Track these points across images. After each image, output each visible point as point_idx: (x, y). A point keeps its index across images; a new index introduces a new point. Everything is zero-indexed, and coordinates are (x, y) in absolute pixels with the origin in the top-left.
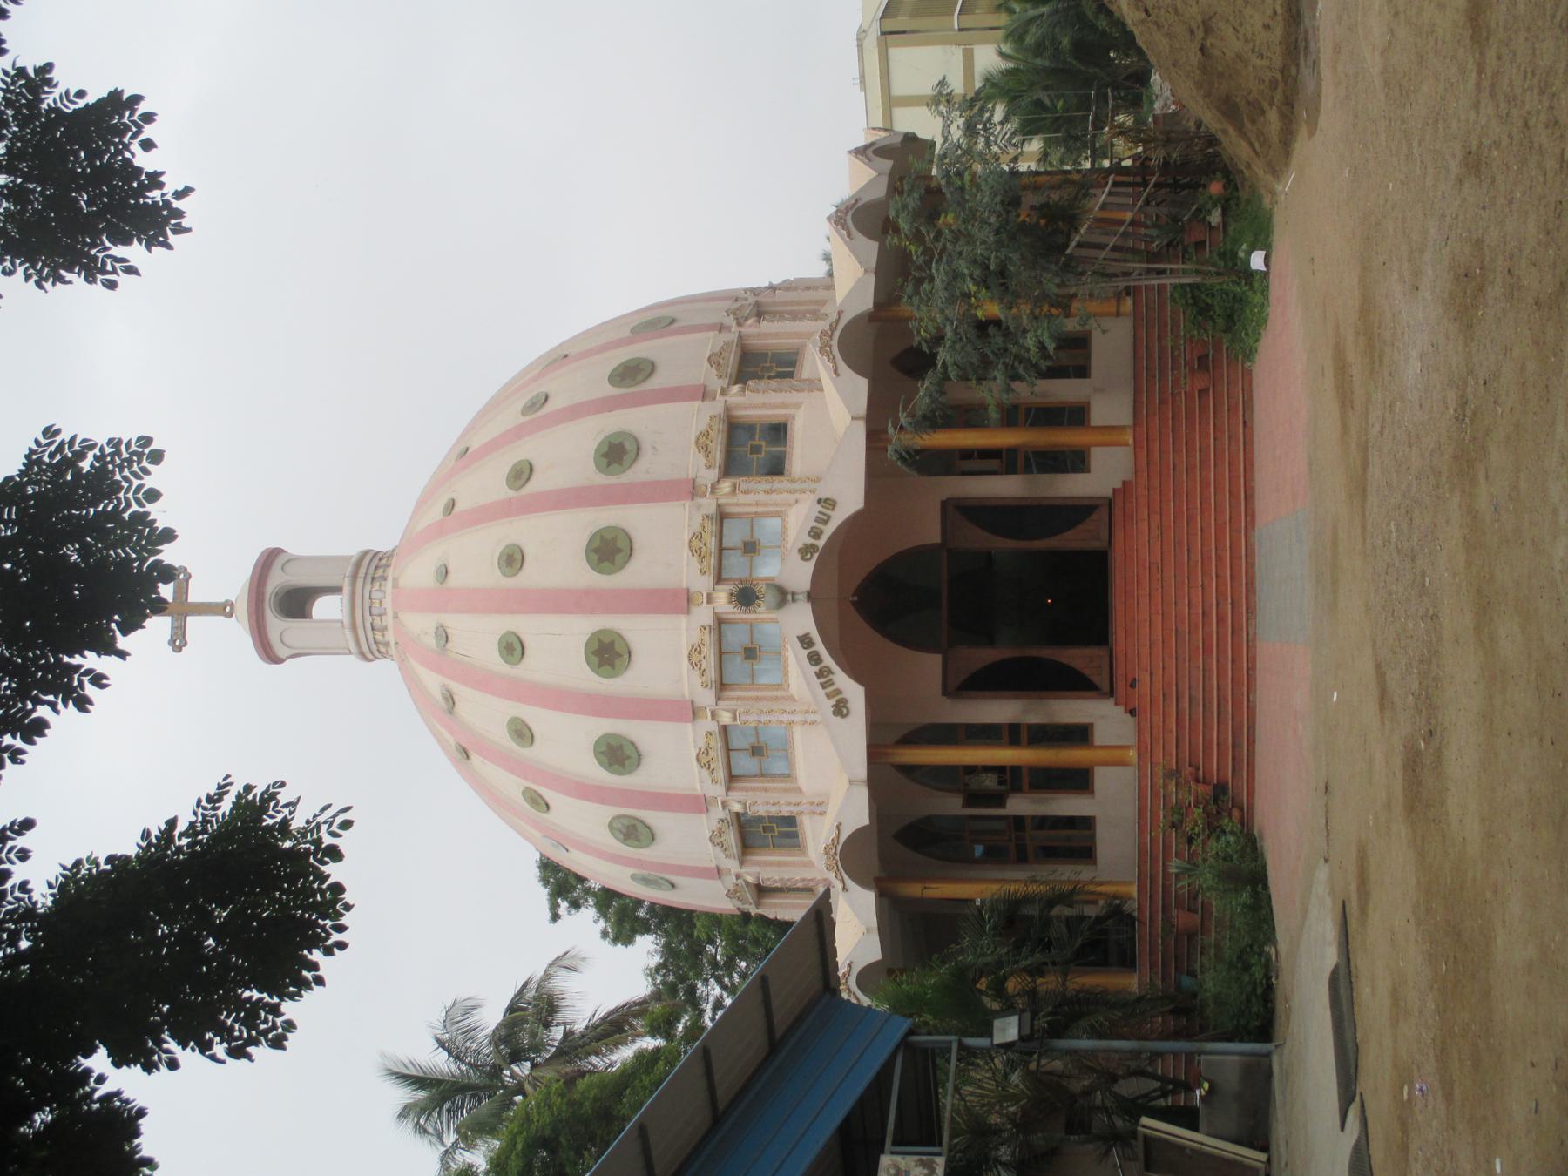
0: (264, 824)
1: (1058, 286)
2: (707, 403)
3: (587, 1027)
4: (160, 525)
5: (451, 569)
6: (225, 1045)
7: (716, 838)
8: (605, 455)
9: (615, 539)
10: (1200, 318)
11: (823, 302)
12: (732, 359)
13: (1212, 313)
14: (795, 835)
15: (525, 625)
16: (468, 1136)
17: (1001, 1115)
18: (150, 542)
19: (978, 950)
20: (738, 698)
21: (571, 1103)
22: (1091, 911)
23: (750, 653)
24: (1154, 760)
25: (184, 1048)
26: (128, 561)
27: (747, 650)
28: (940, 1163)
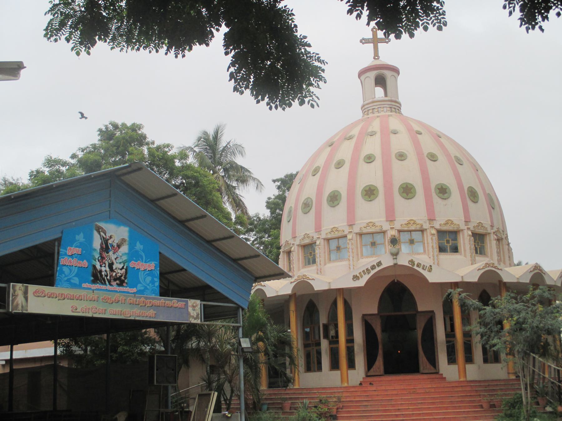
0: (311, 77)
1: (518, 350)
2: (464, 223)
3: (237, 194)
4: (415, 32)
5: (397, 135)
6: (234, 71)
7: (306, 236)
8: (442, 187)
9: (411, 193)
10: (510, 404)
11: (504, 263)
12: (481, 231)
13: (512, 408)
14: (309, 264)
15: (378, 164)
16: (198, 156)
17: (215, 342)
18: (409, 29)
19: (272, 331)
20: (357, 240)
21: (211, 191)
22: (288, 371)
23: (373, 244)
24: (344, 393)
25: (232, 57)
26: (402, 22)
27: (374, 243)
28: (199, 321)
